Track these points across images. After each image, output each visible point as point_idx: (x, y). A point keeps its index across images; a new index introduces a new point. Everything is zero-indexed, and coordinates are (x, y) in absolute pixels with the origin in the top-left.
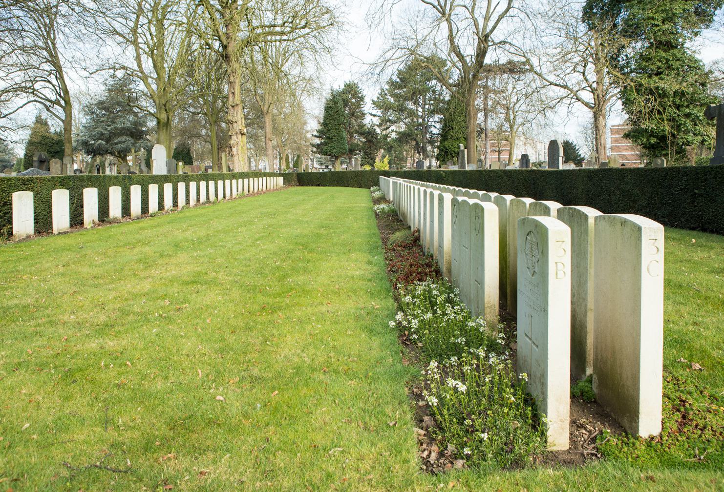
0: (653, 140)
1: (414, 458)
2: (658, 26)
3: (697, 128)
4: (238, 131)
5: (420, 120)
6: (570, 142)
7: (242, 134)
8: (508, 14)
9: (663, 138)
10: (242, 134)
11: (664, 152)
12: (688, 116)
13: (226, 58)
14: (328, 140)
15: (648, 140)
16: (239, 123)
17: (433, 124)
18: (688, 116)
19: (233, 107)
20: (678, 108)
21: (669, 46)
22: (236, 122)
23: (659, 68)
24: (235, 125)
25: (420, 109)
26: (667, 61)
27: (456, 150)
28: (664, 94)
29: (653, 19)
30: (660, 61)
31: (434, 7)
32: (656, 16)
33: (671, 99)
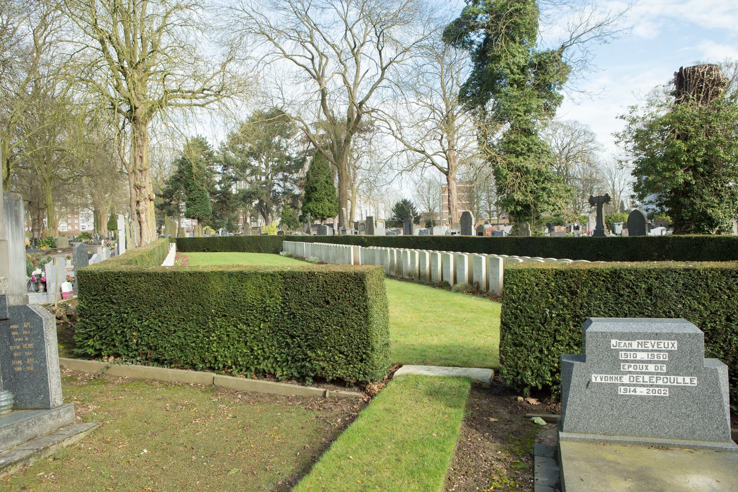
0: (519, 208)
1: (703, 351)
2: (521, 116)
3: (550, 199)
4: (147, 196)
5: (263, 179)
6: (408, 200)
7: (151, 200)
8: (381, 84)
9: (527, 207)
10: (151, 200)
11: (527, 218)
12: (544, 189)
13: (134, 120)
14: (191, 202)
15: (515, 208)
16: (148, 188)
17: (277, 182)
18: (544, 189)
19: (141, 171)
20: (536, 183)
21: (528, 132)
22: (144, 187)
23: (522, 149)
24: (143, 190)
25: (263, 166)
26: (529, 144)
27: (321, 212)
28: (527, 172)
29: (517, 110)
30: (524, 145)
31: (307, 69)
32: (520, 108)
33: (532, 176)
